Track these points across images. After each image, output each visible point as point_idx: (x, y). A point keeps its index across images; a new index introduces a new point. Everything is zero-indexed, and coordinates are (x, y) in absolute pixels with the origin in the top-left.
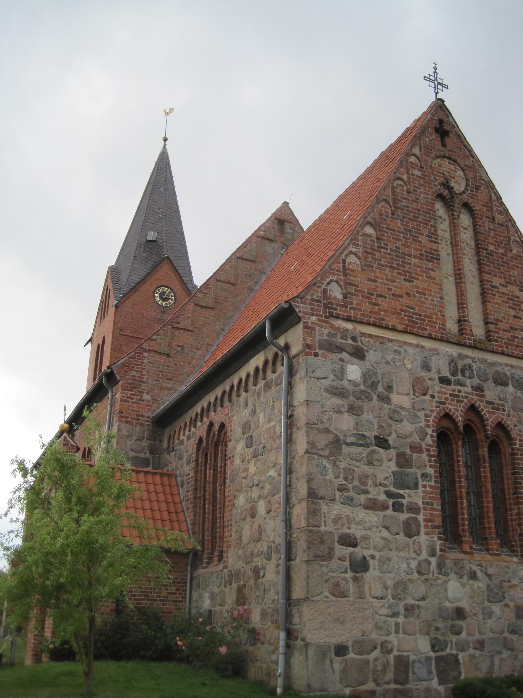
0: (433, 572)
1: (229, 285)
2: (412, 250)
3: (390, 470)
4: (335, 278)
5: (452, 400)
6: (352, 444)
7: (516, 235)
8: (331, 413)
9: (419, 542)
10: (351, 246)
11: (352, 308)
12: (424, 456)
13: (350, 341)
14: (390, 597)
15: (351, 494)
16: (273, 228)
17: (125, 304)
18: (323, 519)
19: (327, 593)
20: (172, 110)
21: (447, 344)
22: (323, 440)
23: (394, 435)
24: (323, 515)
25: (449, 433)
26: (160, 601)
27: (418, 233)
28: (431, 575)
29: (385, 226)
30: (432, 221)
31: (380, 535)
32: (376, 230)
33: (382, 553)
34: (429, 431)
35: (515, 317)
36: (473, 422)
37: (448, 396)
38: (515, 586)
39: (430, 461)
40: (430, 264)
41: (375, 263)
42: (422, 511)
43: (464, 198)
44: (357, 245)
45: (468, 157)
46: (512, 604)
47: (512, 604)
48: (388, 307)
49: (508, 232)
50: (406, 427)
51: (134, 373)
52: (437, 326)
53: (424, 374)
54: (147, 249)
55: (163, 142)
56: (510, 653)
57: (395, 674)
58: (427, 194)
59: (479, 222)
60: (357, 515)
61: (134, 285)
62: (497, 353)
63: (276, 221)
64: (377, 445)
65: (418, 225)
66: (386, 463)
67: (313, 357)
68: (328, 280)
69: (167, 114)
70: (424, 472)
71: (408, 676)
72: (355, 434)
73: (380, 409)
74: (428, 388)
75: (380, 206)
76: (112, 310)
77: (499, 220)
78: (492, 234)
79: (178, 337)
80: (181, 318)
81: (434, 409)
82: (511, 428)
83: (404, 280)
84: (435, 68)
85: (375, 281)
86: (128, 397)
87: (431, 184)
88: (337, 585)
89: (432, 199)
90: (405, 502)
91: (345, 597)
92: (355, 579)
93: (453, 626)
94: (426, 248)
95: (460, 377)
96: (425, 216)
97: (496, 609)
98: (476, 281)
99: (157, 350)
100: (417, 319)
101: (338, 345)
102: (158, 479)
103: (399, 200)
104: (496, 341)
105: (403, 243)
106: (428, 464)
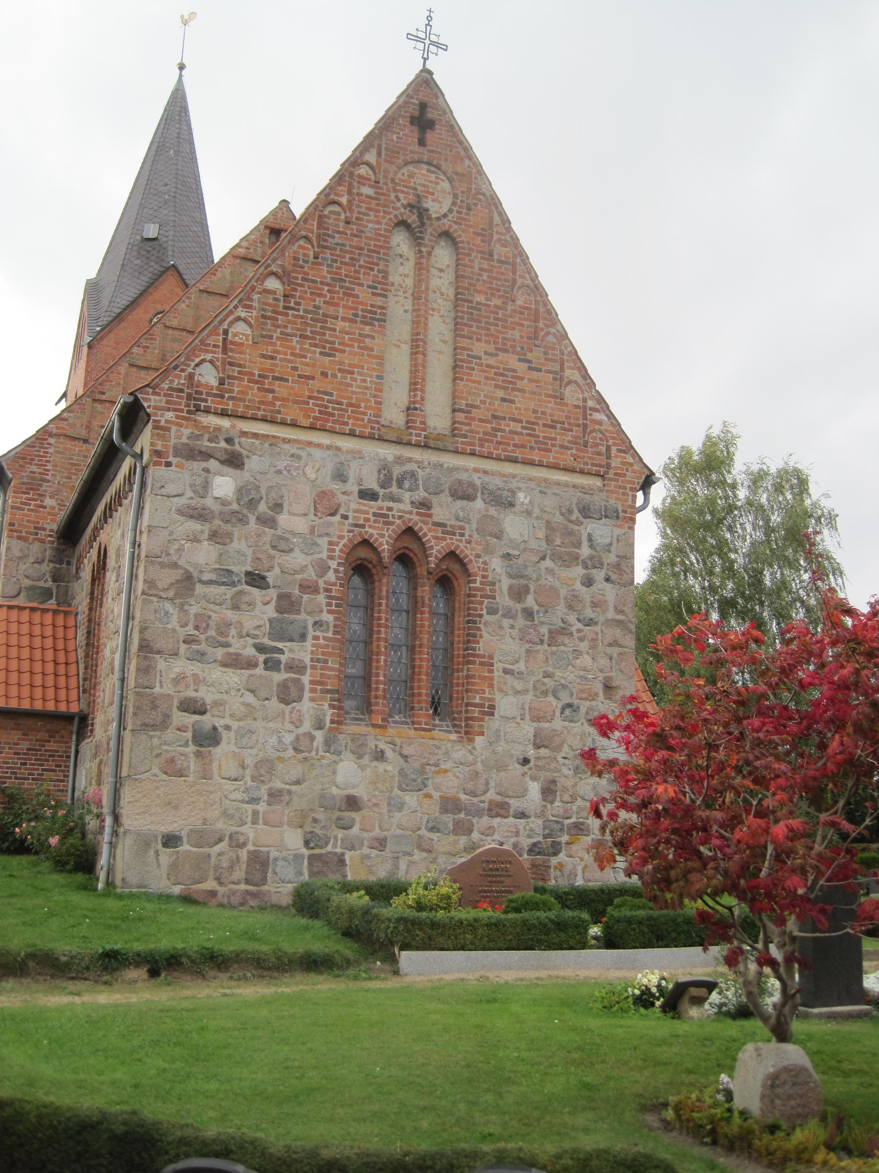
0: (317, 750)
1: (184, 334)
2: (341, 310)
3: (265, 617)
4: (209, 356)
5: (375, 522)
6: (210, 582)
7: (527, 276)
8: (183, 542)
9: (299, 711)
10: (240, 309)
11: (230, 398)
12: (321, 598)
13: (223, 444)
14: (248, 778)
15: (203, 647)
16: (261, 242)
17: (104, 342)
18: (158, 678)
19: (156, 770)
20: (193, 15)
21: (380, 443)
22: (167, 577)
23: (277, 570)
24: (158, 674)
25: (370, 566)
26: (33, 779)
27: (354, 284)
28: (313, 753)
29: (300, 276)
30: (382, 263)
31: (241, 700)
32: (283, 283)
33: (241, 724)
34: (333, 564)
35: (504, 400)
36: (411, 551)
37: (370, 516)
38: (446, 771)
39: (329, 604)
40: (368, 328)
41: (276, 331)
42: (309, 670)
43: (444, 224)
44: (250, 307)
45: (462, 160)
46: (436, 795)
47: (436, 795)
48: (290, 394)
49: (514, 273)
50: (298, 559)
51: (34, 468)
52: (366, 418)
53: (336, 486)
54: (143, 253)
56: (425, 854)
57: (247, 872)
58: (379, 223)
59: (464, 259)
60: (210, 673)
61: (118, 311)
62: (463, 453)
63: (268, 232)
64: (247, 583)
65: (356, 272)
66: (259, 608)
67: (163, 467)
68: (197, 360)
69: (185, 23)
70: (317, 619)
71: (266, 877)
72: (215, 570)
73: (259, 536)
74: (339, 505)
75: (295, 247)
76: (85, 350)
77: (500, 255)
78: (485, 278)
79: (102, 413)
80: (107, 386)
81: (346, 534)
82: (471, 560)
83: (321, 353)
84: (429, 18)
85: (273, 358)
86: (22, 503)
87: (388, 207)
88: (172, 760)
89: (386, 230)
90: (283, 658)
91: (181, 776)
92: (198, 754)
93: (339, 818)
94: (365, 304)
95: (394, 489)
96: (369, 256)
97: (411, 800)
98: (448, 349)
99: (69, 433)
100: (334, 409)
101: (203, 449)
102: (48, 618)
103: (329, 236)
104: (465, 436)
105: (327, 299)
106: (325, 609)
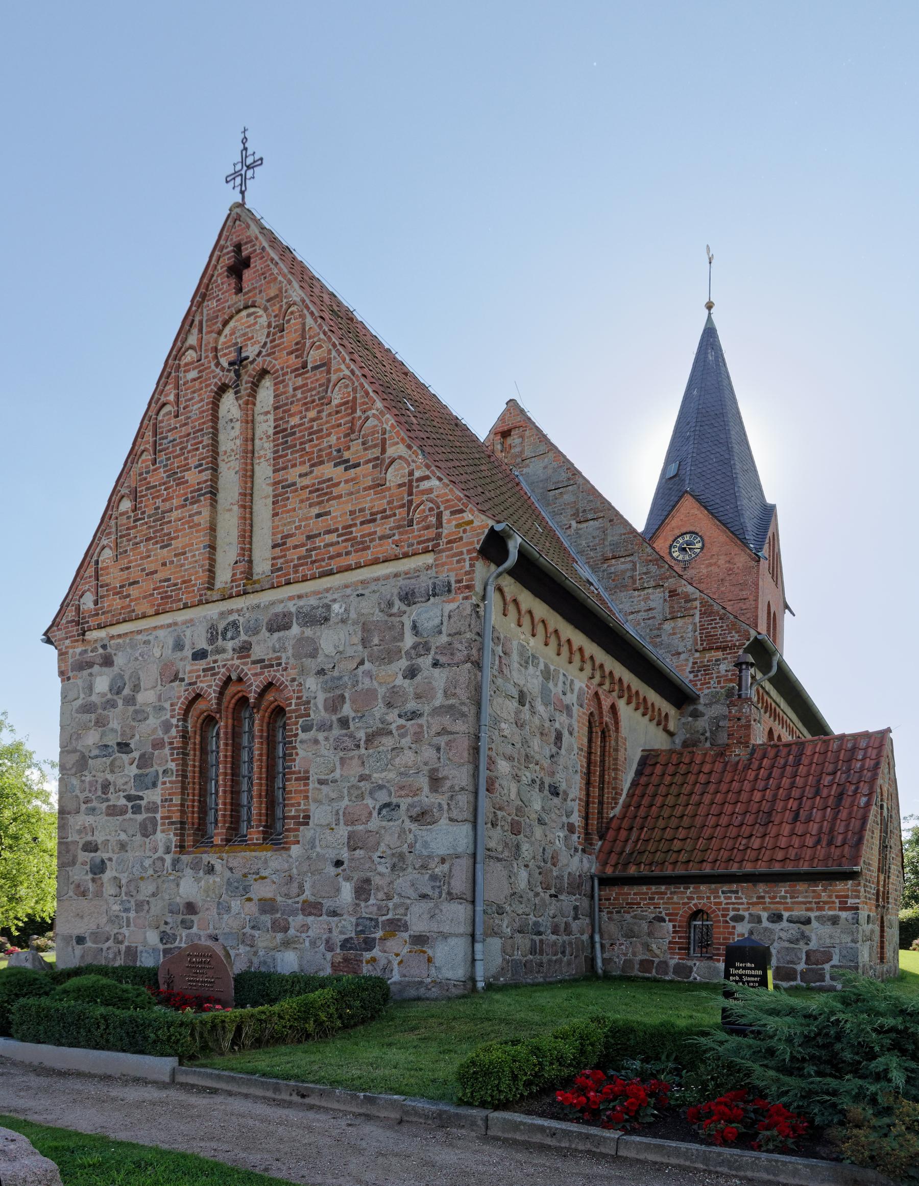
6: (96, 757)
38: (265, 878)
39: (172, 754)
42: (160, 809)
55: (707, 311)
92: (93, 880)
